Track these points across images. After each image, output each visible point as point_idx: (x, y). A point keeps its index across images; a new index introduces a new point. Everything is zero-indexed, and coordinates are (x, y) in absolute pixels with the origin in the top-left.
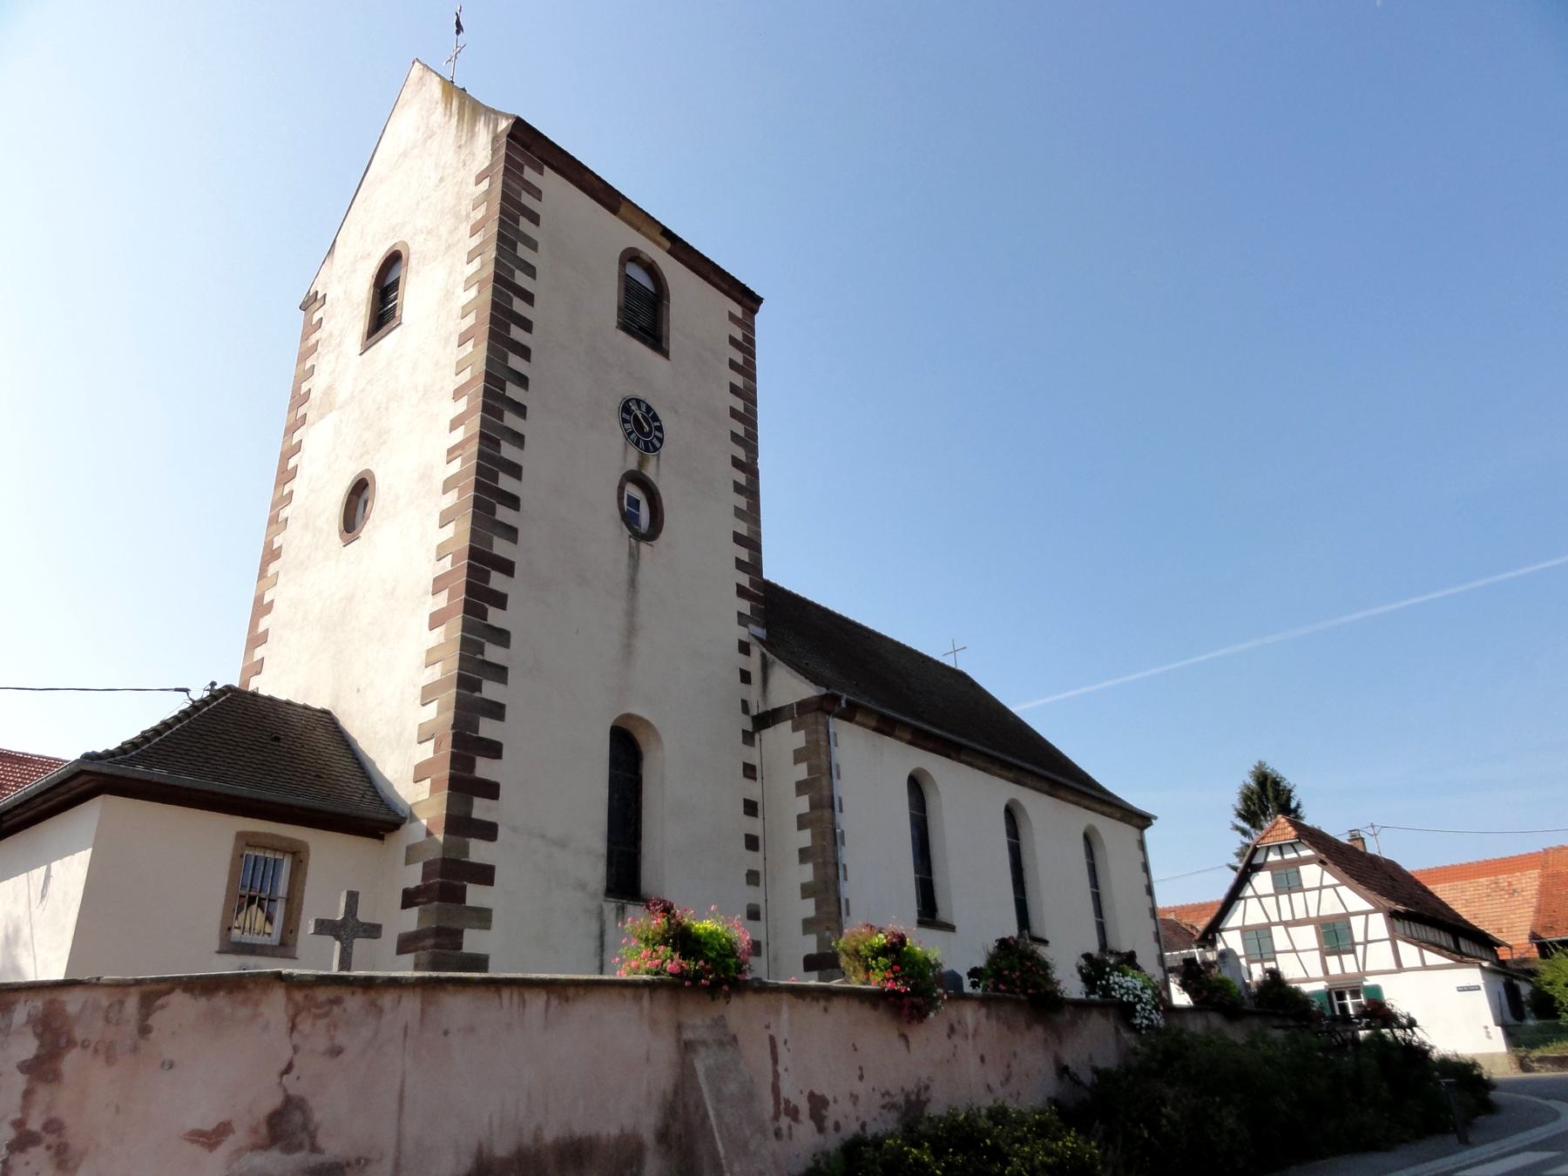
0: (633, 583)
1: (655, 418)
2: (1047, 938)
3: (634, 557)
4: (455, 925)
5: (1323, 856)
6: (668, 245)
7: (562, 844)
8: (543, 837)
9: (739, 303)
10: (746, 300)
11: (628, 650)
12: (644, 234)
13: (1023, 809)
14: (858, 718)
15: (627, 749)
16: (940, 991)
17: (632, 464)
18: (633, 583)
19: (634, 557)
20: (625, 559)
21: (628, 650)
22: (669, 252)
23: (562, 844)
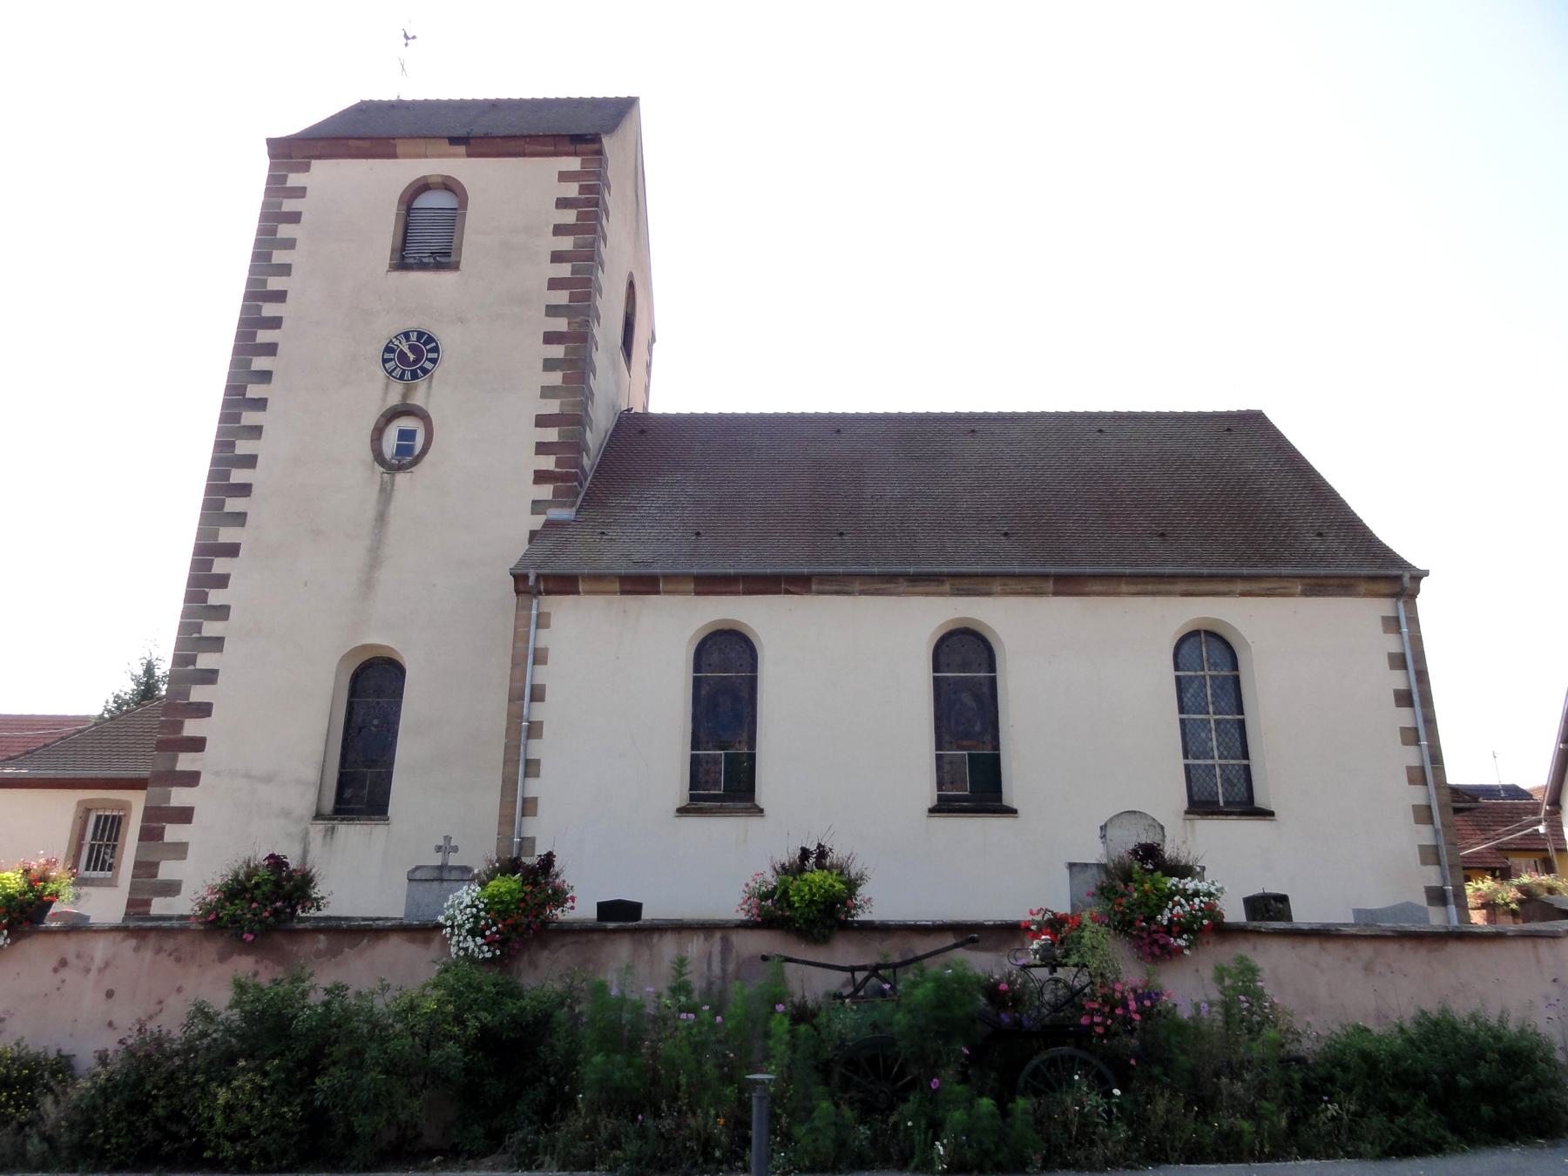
0: (381, 518)
1: (430, 339)
2: (1015, 806)
3: (386, 493)
4: (151, 859)
5: (1189, 988)
6: (462, 149)
7: (268, 779)
8: (248, 776)
9: (575, 154)
10: (580, 147)
11: (368, 584)
12: (433, 156)
13: (1216, 621)
14: (814, 587)
15: (374, 686)
16: (453, 950)
17: (394, 399)
18: (381, 518)
19: (386, 493)
20: (373, 494)
21: (368, 584)
22: (469, 155)
23: (268, 779)
